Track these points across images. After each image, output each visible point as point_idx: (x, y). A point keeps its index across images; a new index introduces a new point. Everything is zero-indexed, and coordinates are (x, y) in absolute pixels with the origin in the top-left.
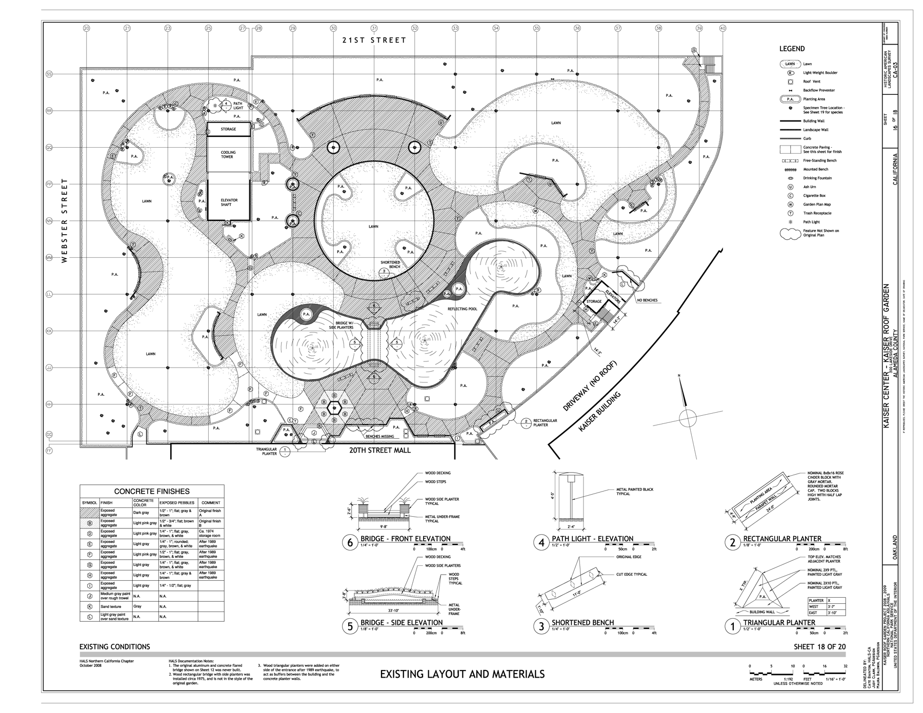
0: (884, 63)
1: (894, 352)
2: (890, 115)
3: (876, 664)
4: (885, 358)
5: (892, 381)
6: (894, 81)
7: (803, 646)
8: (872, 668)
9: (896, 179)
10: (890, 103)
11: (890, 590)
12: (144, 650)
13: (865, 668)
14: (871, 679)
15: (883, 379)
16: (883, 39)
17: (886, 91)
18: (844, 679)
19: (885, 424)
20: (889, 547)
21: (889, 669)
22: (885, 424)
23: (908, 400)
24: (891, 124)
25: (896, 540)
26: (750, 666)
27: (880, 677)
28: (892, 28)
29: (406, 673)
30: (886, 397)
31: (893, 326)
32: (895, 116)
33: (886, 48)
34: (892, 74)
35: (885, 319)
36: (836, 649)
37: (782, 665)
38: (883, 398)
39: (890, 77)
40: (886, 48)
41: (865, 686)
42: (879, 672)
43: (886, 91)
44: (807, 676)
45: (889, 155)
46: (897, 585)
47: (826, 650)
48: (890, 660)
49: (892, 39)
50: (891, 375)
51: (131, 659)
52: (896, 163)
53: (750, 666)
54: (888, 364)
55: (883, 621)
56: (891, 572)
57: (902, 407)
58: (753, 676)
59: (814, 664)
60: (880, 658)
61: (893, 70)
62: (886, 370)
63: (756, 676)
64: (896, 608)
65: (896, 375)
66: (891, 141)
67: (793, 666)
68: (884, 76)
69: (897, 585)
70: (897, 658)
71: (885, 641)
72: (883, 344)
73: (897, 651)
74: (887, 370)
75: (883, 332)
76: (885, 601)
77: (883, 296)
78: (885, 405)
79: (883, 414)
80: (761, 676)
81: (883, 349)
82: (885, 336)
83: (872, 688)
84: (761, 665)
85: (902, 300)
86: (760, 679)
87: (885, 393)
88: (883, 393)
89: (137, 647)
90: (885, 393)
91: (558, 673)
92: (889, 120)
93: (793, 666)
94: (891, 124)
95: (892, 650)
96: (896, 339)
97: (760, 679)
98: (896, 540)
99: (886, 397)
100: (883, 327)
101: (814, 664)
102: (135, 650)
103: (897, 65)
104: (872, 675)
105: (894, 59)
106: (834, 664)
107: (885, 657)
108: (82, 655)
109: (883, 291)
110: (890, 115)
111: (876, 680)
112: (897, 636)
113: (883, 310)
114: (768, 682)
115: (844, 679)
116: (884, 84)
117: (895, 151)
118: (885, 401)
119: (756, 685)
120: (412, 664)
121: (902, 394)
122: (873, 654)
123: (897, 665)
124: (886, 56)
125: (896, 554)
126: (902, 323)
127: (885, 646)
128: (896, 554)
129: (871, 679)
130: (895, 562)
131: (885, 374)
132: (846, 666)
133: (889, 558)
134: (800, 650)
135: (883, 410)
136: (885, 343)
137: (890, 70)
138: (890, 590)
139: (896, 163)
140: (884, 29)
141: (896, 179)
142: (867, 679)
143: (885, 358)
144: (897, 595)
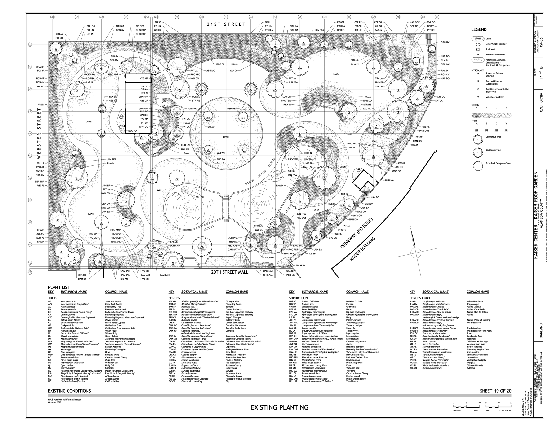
0: (535, 38)
1: (541, 213)
2: (538, 70)
3: (529, 402)
4: (535, 216)
5: (540, 230)
6: (540, 49)
7: (485, 391)
8: (527, 404)
9: (542, 108)
10: (538, 63)
11: (538, 356)
12: (87, 393)
13: (523, 404)
14: (527, 411)
15: (534, 229)
16: (534, 24)
17: (536, 55)
18: (510, 410)
19: (535, 256)
20: (538, 330)
21: (538, 405)
22: (535, 256)
23: (549, 242)
25: (542, 326)
26: (453, 403)
27: (532, 409)
28: (539, 17)
29: (298, 407)
30: (536, 240)
31: (540, 197)
32: (541, 70)
33: (536, 29)
34: (539, 45)
35: (535, 193)
36: (505, 392)
37: (473, 402)
38: (534, 240)
39: (538, 47)
40: (536, 29)
41: (523, 415)
42: (531, 406)
43: (536, 55)
44: (488, 409)
45: (538, 94)
46: (542, 354)
47: (499, 393)
48: (538, 399)
49: (539, 23)
50: (539, 227)
51: (79, 398)
52: (542, 99)
53: (453, 403)
54: (537, 220)
55: (534, 376)
56: (538, 346)
57: (545, 246)
58: (455, 409)
59: (492, 402)
60: (532, 398)
61: (540, 42)
62: (535, 224)
63: (457, 409)
64: (542, 367)
65: (542, 227)
66: (538, 85)
67: (480, 403)
68: (534, 46)
69: (542, 354)
70: (542, 398)
71: (535, 387)
72: (534, 208)
73: (542, 394)
74: (536, 224)
75: (534, 201)
76: (535, 364)
77: (534, 179)
78: (535, 245)
79: (534, 250)
80: (460, 408)
81: (534, 211)
82: (535, 203)
83: (527, 416)
84: (460, 402)
85: (545, 181)
86: (460, 410)
87: (535, 237)
88: (534, 238)
89: (83, 391)
90: (535, 237)
91: (316, 407)
92: (538, 73)
93: (480, 403)
95: (539, 393)
96: (542, 205)
97: (460, 410)
98: (542, 326)
99: (536, 240)
100: (534, 198)
101: (492, 402)
102: (81, 393)
103: (542, 39)
104: (527, 408)
105: (540, 36)
106: (504, 401)
107: (535, 397)
108: (50, 396)
109: (534, 176)
110: (538, 70)
111: (529, 411)
112: (542, 384)
113: (534, 187)
114: (464, 412)
115: (510, 410)
116: (534, 51)
117: (541, 91)
118: (535, 243)
119: (457, 414)
120: (270, 401)
121: (545, 238)
122: (528, 396)
123: (542, 402)
124: (536, 34)
125: (542, 335)
126: (545, 195)
127: (535, 391)
128: (542, 335)
129: (527, 411)
130: (541, 340)
131: (535, 226)
132: (511, 403)
133: (537, 337)
134: (484, 393)
135: (534, 248)
136: (535, 208)
137: (538, 42)
138: (538, 356)
139: (542, 99)
140: (535, 18)
141: (542, 108)
142: (524, 411)
143: (535, 216)
144: (542, 360)
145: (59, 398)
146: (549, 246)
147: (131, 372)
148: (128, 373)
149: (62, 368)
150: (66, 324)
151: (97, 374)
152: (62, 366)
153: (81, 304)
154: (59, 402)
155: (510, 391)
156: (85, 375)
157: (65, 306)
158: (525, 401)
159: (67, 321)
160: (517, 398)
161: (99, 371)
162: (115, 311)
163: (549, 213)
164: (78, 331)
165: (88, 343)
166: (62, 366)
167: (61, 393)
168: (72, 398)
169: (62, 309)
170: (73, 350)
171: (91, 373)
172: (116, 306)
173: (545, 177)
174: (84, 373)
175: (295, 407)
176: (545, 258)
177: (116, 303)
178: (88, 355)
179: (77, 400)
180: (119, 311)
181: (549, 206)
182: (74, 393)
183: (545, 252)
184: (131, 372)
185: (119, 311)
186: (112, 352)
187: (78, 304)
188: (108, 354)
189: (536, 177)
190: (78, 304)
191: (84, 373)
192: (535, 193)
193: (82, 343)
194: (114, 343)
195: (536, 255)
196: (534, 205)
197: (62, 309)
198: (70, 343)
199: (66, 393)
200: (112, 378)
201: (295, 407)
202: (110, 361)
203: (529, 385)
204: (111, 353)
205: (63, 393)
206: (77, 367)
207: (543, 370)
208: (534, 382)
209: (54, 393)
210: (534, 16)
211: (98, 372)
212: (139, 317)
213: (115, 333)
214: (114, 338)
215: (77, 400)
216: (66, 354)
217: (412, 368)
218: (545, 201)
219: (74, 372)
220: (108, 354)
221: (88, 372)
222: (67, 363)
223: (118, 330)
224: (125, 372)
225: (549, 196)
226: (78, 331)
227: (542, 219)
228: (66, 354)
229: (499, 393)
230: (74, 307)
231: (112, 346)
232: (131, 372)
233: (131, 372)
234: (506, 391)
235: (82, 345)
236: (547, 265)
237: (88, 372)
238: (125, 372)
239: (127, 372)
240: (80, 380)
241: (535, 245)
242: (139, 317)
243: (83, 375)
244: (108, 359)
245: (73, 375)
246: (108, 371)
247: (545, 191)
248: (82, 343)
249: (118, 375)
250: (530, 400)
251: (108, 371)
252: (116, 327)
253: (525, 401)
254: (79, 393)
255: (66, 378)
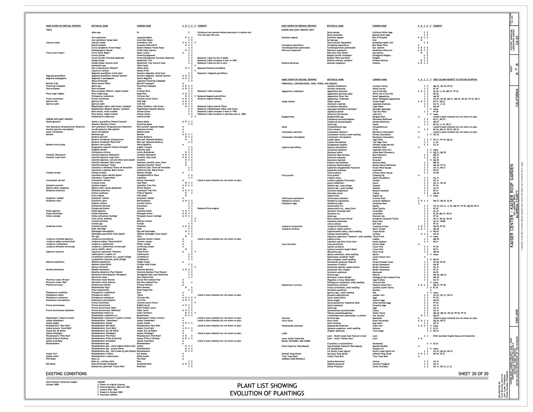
0: (511, 37)
1: (516, 203)
2: (514, 67)
3: (506, 384)
4: (511, 207)
5: (515, 220)
6: (516, 47)
7: (463, 373)
8: (504, 386)
9: (518, 104)
10: (514, 60)
11: (514, 341)
12: (83, 376)
13: (499, 386)
14: (503, 393)
15: (510, 219)
16: (510, 23)
17: (512, 52)
19: (511, 245)
20: (514, 316)
21: (513, 387)
22: (511, 245)
23: (524, 231)
24: (514, 72)
25: (517, 312)
27: (508, 391)
28: (515, 16)
29: (291, 393)
30: (512, 229)
31: (515, 188)
32: (517, 67)
33: (512, 28)
34: (515, 43)
35: (511, 184)
36: (483, 375)
38: (510, 230)
39: (514, 45)
40: (512, 28)
41: (499, 396)
42: (508, 388)
43: (512, 52)
45: (513, 90)
46: (518, 338)
47: (477, 375)
48: (514, 381)
49: (515, 22)
50: (514, 217)
51: (76, 381)
52: (517, 94)
54: (513, 210)
55: (510, 359)
56: (514, 331)
57: (521, 235)
60: (508, 380)
61: (515, 40)
62: (511, 214)
64: (517, 351)
65: (518, 217)
66: (514, 81)
68: (510, 44)
69: (518, 338)
70: (518, 380)
71: (511, 370)
72: (510, 199)
73: (518, 376)
74: (512, 214)
75: (510, 192)
76: (511, 348)
77: (510, 171)
78: (511, 234)
79: (510, 239)
81: (510, 201)
82: (511, 194)
83: (504, 398)
85: (521, 173)
87: (511, 227)
88: (510, 227)
89: (79, 374)
90: (511, 227)
92: (513, 69)
94: (514, 72)
95: (515, 376)
96: (518, 196)
98: (517, 312)
99: (512, 229)
100: (510, 189)
102: (78, 376)
103: (518, 38)
104: (504, 390)
105: (516, 34)
107: (511, 379)
108: (47, 378)
109: (510, 168)
110: (514, 67)
111: (506, 393)
112: (518, 368)
113: (510, 179)
116: (510, 49)
117: (517, 87)
118: (511, 232)
121: (521, 228)
122: (504, 378)
123: (518, 384)
124: (512, 33)
125: (517, 320)
126: (521, 187)
127: (511, 374)
128: (517, 320)
129: (503, 393)
130: (517, 325)
131: (511, 216)
133: (513, 322)
134: (462, 376)
135: (510, 237)
136: (511, 198)
138: (514, 341)
139: (517, 94)
140: (511, 17)
141: (518, 104)
142: (501, 393)
143: (511, 207)
144: (518, 344)
145: (57, 381)
146: (524, 235)
147: (162, 108)
148: (159, 109)
149: (93, 104)
150: (96, 52)
151: (126, 109)
152: (93, 101)
153: (111, 40)
154: (56, 385)
155: (487, 374)
156: (115, 109)
157: (95, 41)
158: (501, 384)
159: (97, 49)
160: (495, 378)
161: (128, 106)
162: (146, 46)
163: (525, 203)
164: (107, 66)
165: (117, 75)
166: (93, 101)
167: (59, 376)
168: (69, 381)
169: (92, 45)
170: (103, 86)
171: (121, 108)
172: (147, 41)
173: (521, 169)
174: (114, 109)
175: (288, 393)
176: (520, 246)
177: (147, 39)
178: (118, 91)
179: (73, 382)
180: (150, 47)
181: (524, 196)
182: (71, 376)
183: (521, 241)
184: (162, 108)
185: (150, 47)
186: (144, 89)
187: (108, 40)
188: (139, 90)
189: (512, 169)
190: (108, 40)
191: (114, 109)
192: (511, 184)
193: (111, 75)
194: (146, 75)
195: (512, 243)
196: (510, 196)
197: (92, 45)
198: (100, 75)
199: (63, 375)
200: (144, 113)
201: (288, 393)
202: (142, 97)
203: (505, 368)
204: (142, 90)
205: (60, 376)
206: (106, 103)
207: (518, 353)
208: (511, 365)
209: (51, 376)
210: (510, 15)
211: (127, 108)
212: (169, 58)
213: (146, 67)
214: (145, 72)
215: (73, 382)
216: (96, 90)
217: (435, 173)
218: (521, 192)
219: (104, 108)
220: (139, 90)
221: (117, 108)
222: (97, 96)
223: (149, 65)
224: (155, 108)
225: (524, 187)
226: (107, 66)
227: (518, 210)
228: (96, 90)
229: (477, 375)
230: (104, 43)
231: (143, 77)
232: (161, 108)
233: (161, 108)
234: (483, 374)
235: (112, 77)
236: (523, 253)
237: (117, 108)
238: (155, 108)
239: (157, 108)
240: (110, 115)
241: (511, 234)
242: (169, 58)
243: (113, 110)
244: (139, 93)
245: (103, 111)
246: (139, 106)
247: (521, 183)
248: (111, 75)
249: (149, 110)
250: (506, 382)
251: (139, 106)
252: (147, 62)
253: (501, 384)
254: (76, 376)
255: (96, 113)
